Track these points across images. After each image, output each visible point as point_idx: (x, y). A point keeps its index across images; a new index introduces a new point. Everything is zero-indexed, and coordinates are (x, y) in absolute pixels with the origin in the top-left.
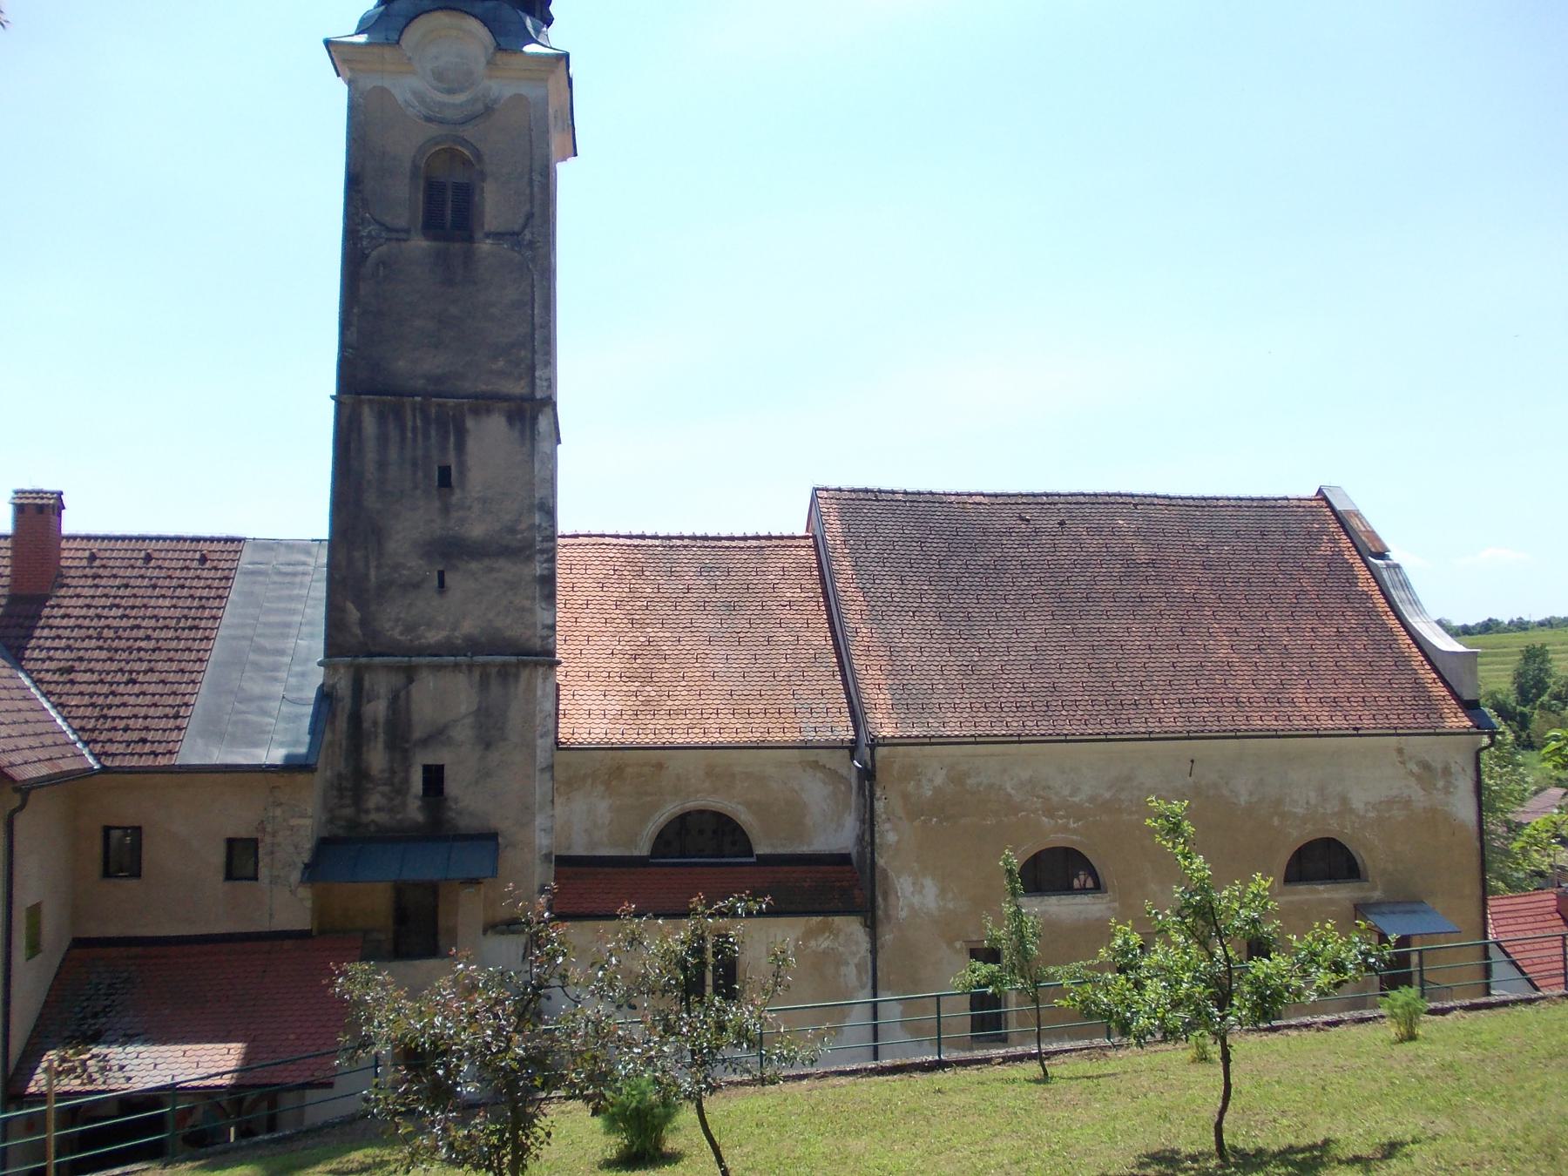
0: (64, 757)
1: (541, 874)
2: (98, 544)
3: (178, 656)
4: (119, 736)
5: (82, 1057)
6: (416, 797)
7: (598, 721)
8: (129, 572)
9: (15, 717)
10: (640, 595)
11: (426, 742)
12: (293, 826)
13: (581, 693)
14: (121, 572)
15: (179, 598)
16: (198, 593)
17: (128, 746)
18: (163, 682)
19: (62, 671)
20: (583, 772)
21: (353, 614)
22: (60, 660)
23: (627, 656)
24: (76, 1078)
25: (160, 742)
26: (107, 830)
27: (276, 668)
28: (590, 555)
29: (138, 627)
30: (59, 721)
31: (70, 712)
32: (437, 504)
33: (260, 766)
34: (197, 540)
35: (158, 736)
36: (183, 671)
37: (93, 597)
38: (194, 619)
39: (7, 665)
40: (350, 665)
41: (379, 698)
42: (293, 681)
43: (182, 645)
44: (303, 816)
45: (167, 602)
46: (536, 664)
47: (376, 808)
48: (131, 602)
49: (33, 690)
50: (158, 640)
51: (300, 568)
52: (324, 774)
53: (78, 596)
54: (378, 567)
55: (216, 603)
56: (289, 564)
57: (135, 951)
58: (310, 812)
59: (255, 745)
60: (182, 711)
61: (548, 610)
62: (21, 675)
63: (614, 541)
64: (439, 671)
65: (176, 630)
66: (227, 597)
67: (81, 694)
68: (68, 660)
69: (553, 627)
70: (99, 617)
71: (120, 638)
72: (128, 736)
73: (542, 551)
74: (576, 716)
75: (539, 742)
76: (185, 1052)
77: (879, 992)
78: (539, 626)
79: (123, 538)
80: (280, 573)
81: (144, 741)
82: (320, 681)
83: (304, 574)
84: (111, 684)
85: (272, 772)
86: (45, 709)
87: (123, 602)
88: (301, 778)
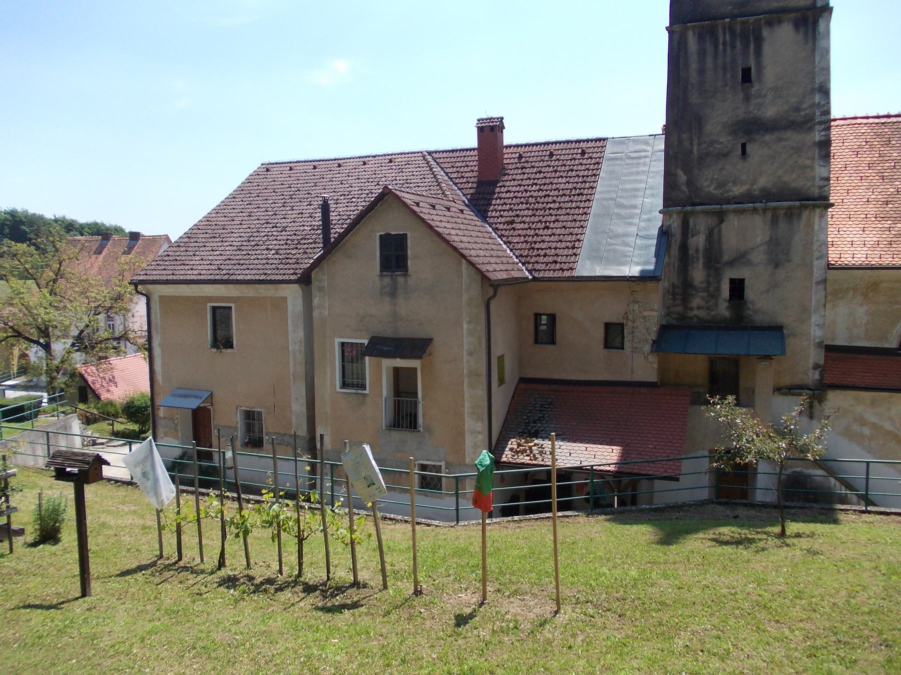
0: (513, 270)
1: (815, 356)
2: (523, 149)
3: (572, 212)
4: (541, 259)
5: (529, 444)
6: (725, 300)
7: (859, 249)
8: (541, 164)
9: (487, 246)
10: (888, 158)
11: (731, 263)
12: (645, 317)
13: (845, 229)
14: (537, 164)
15: (571, 177)
16: (581, 173)
17: (547, 265)
18: (564, 227)
19: (508, 223)
20: (846, 286)
21: (682, 177)
22: (507, 217)
23: (880, 203)
24: (527, 456)
25: (565, 263)
26: (537, 316)
27: (632, 216)
28: (846, 132)
29: (548, 196)
30: (508, 251)
31: (514, 246)
32: (741, 95)
33: (625, 277)
34: (579, 141)
35: (564, 259)
36: (575, 220)
37: (522, 180)
38: (580, 189)
39: (480, 220)
40: (680, 212)
41: (699, 234)
42: (643, 224)
43: (574, 205)
44: (653, 310)
45: (564, 180)
46: (814, 207)
47: (697, 306)
48: (543, 181)
49: (493, 234)
50: (560, 203)
51: (643, 154)
52: (664, 284)
53: (514, 180)
54: (699, 144)
55: (593, 179)
56: (636, 152)
57: (555, 387)
58: (656, 308)
59: (622, 264)
60: (577, 244)
61: (824, 166)
62: (487, 226)
63: (865, 121)
64: (742, 214)
65: (570, 196)
66: (599, 175)
67: (519, 235)
68: (511, 217)
69: (828, 179)
70: (526, 191)
71: (538, 203)
72: (546, 259)
73: (821, 123)
74: (842, 246)
75: (816, 263)
76: (587, 448)
77: (158, 439)
78: (818, 179)
79: (537, 144)
80: (630, 158)
81: (556, 262)
82: (660, 224)
83: (646, 157)
84: (535, 229)
85: (633, 281)
86: (500, 244)
87: (539, 182)
88: (651, 285)
